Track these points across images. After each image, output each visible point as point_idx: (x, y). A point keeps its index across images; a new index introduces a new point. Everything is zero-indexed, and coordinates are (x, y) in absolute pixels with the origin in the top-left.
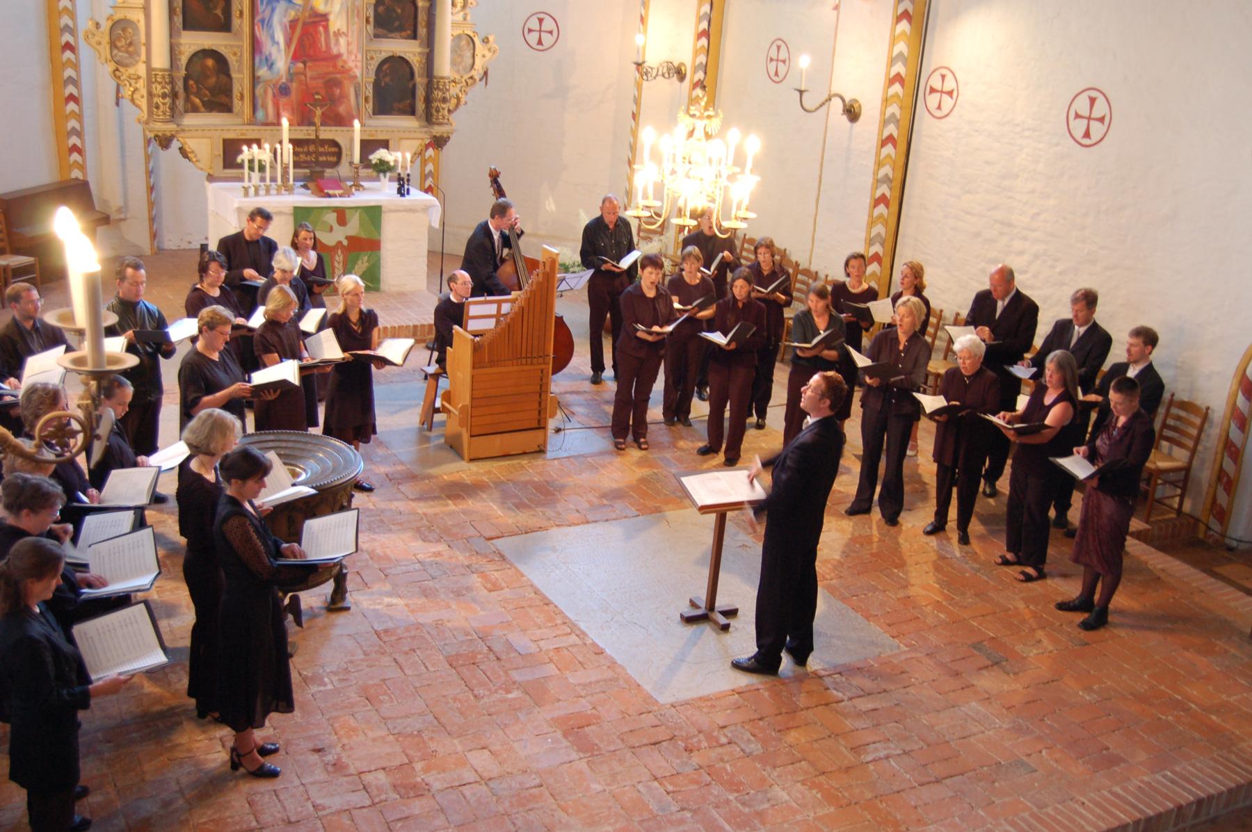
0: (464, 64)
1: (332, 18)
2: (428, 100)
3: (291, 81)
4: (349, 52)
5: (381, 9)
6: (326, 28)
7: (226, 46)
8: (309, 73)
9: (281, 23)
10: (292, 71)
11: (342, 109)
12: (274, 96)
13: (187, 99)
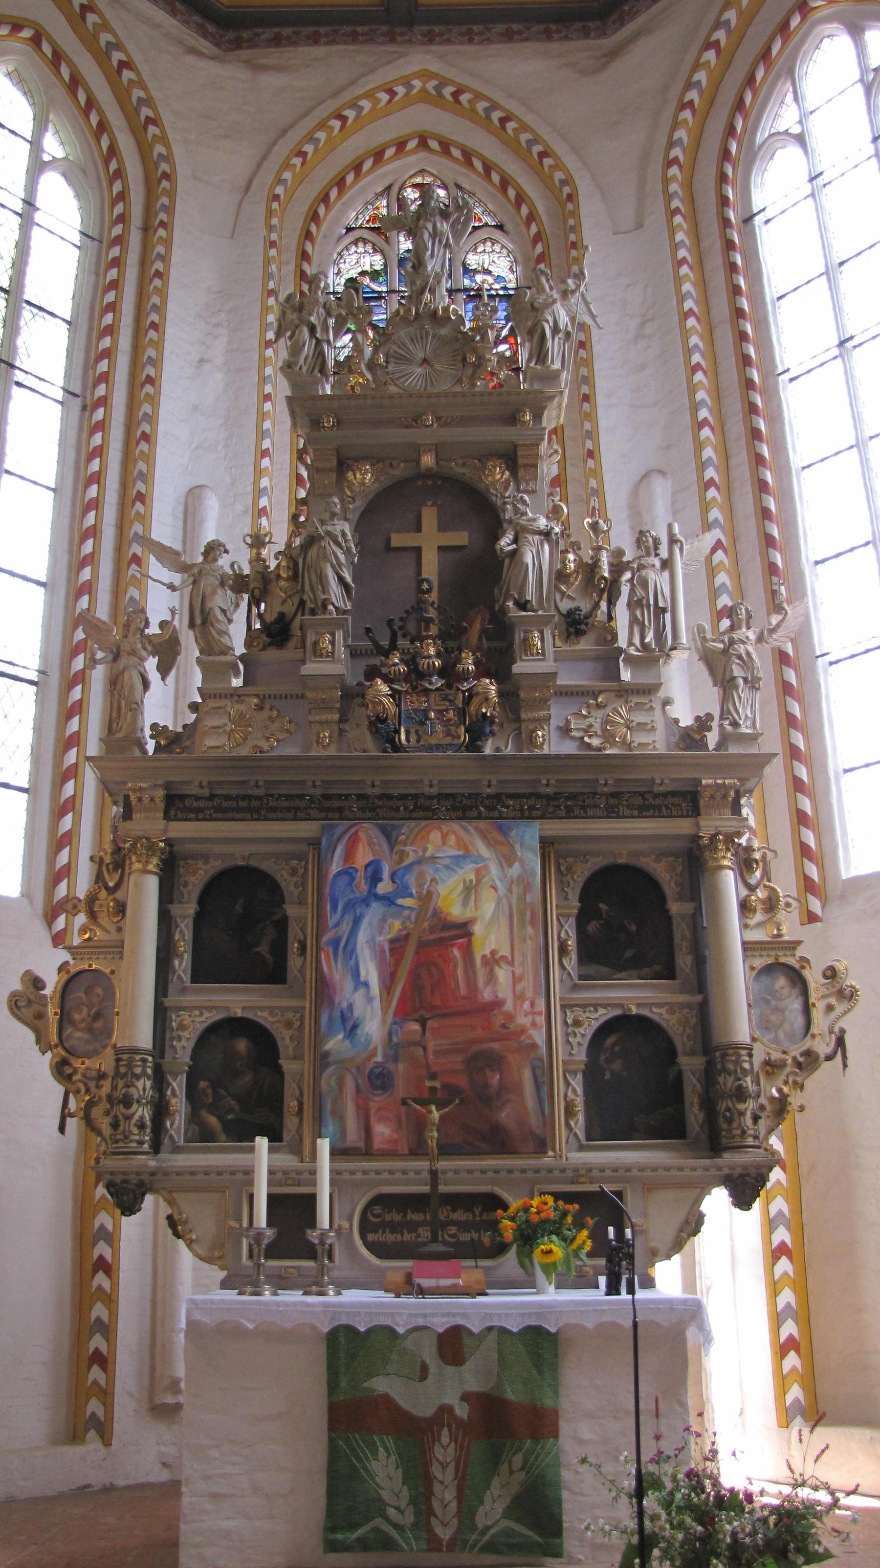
0: (787, 1027)
1: (478, 929)
2: (709, 1104)
3: (395, 1060)
4: (519, 997)
5: (593, 927)
6: (468, 951)
7: (271, 1010)
8: (431, 1044)
9: (371, 942)
10: (395, 1039)
11: (505, 1116)
12: (358, 1091)
13: (194, 1117)
